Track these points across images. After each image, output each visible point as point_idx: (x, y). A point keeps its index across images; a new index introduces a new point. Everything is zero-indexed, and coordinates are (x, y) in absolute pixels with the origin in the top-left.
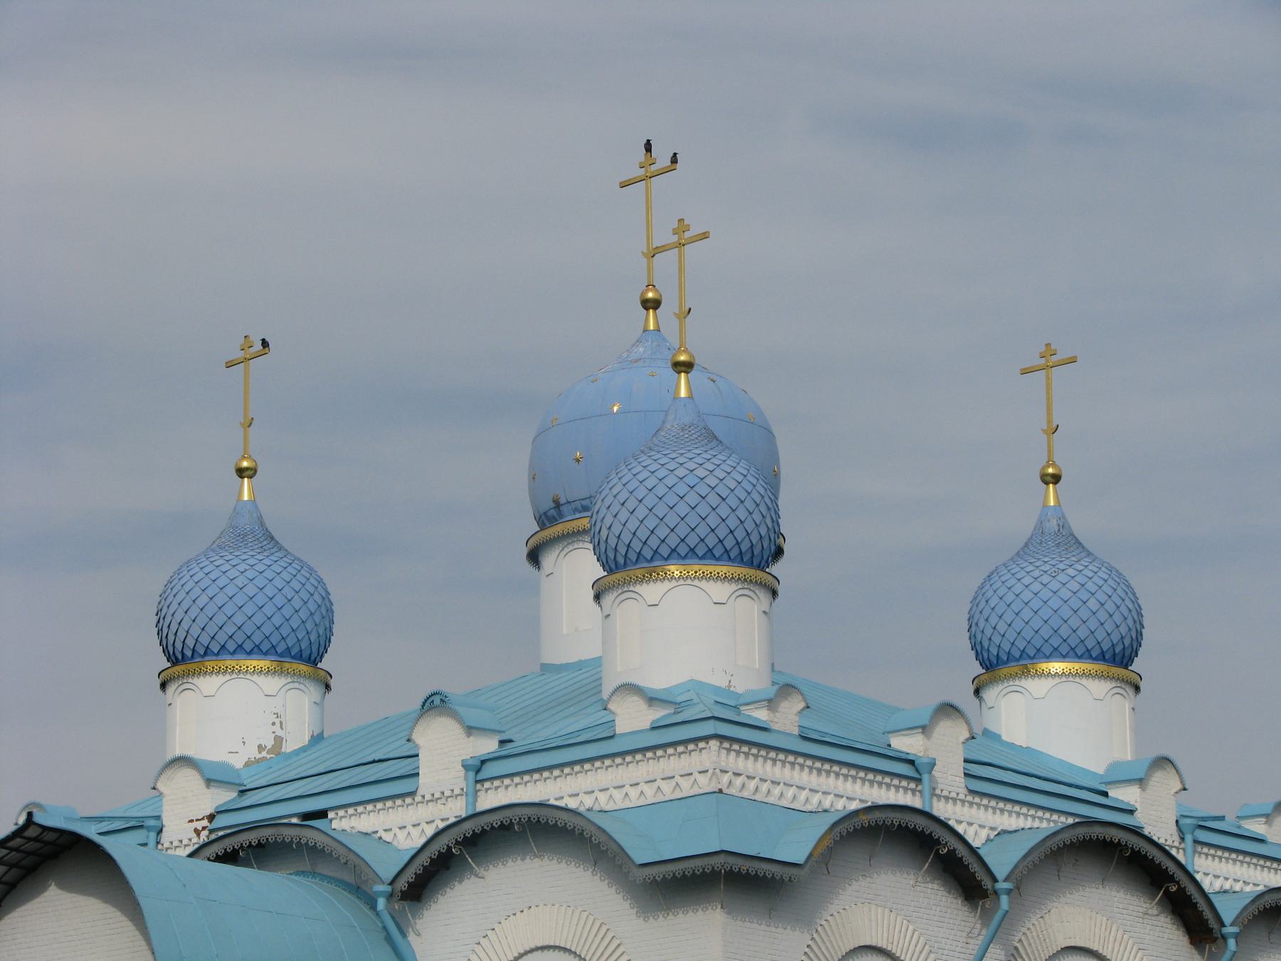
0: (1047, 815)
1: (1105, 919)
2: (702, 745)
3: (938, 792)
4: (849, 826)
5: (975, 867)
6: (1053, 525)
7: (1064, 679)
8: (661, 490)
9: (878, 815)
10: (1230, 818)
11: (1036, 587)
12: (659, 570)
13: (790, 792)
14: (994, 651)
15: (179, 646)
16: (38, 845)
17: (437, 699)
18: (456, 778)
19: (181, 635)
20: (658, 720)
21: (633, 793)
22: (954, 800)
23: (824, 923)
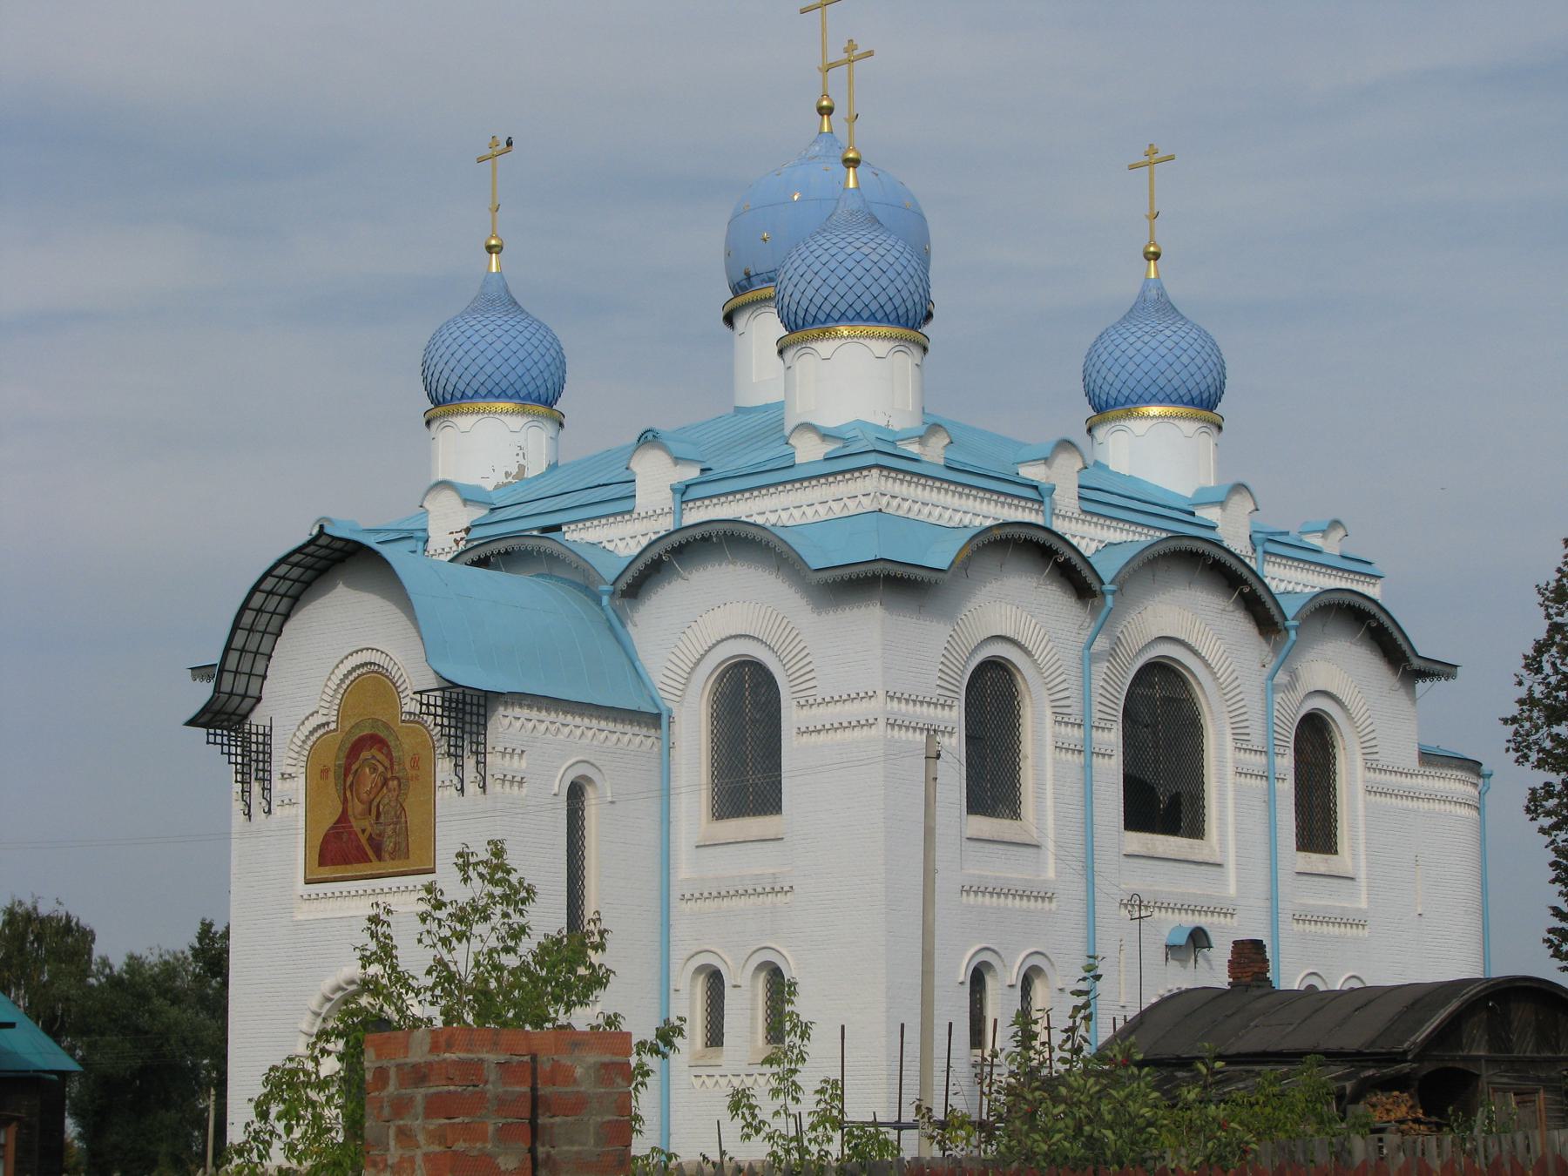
0: (1145, 531)
2: (865, 473)
3: (1057, 511)
4: (984, 539)
5: (1086, 572)
7: (1160, 420)
8: (833, 265)
10: (1294, 533)
11: (1139, 345)
13: (937, 512)
15: (440, 391)
16: (328, 551)
17: (650, 436)
18: (666, 499)
21: (810, 511)
23: (963, 617)
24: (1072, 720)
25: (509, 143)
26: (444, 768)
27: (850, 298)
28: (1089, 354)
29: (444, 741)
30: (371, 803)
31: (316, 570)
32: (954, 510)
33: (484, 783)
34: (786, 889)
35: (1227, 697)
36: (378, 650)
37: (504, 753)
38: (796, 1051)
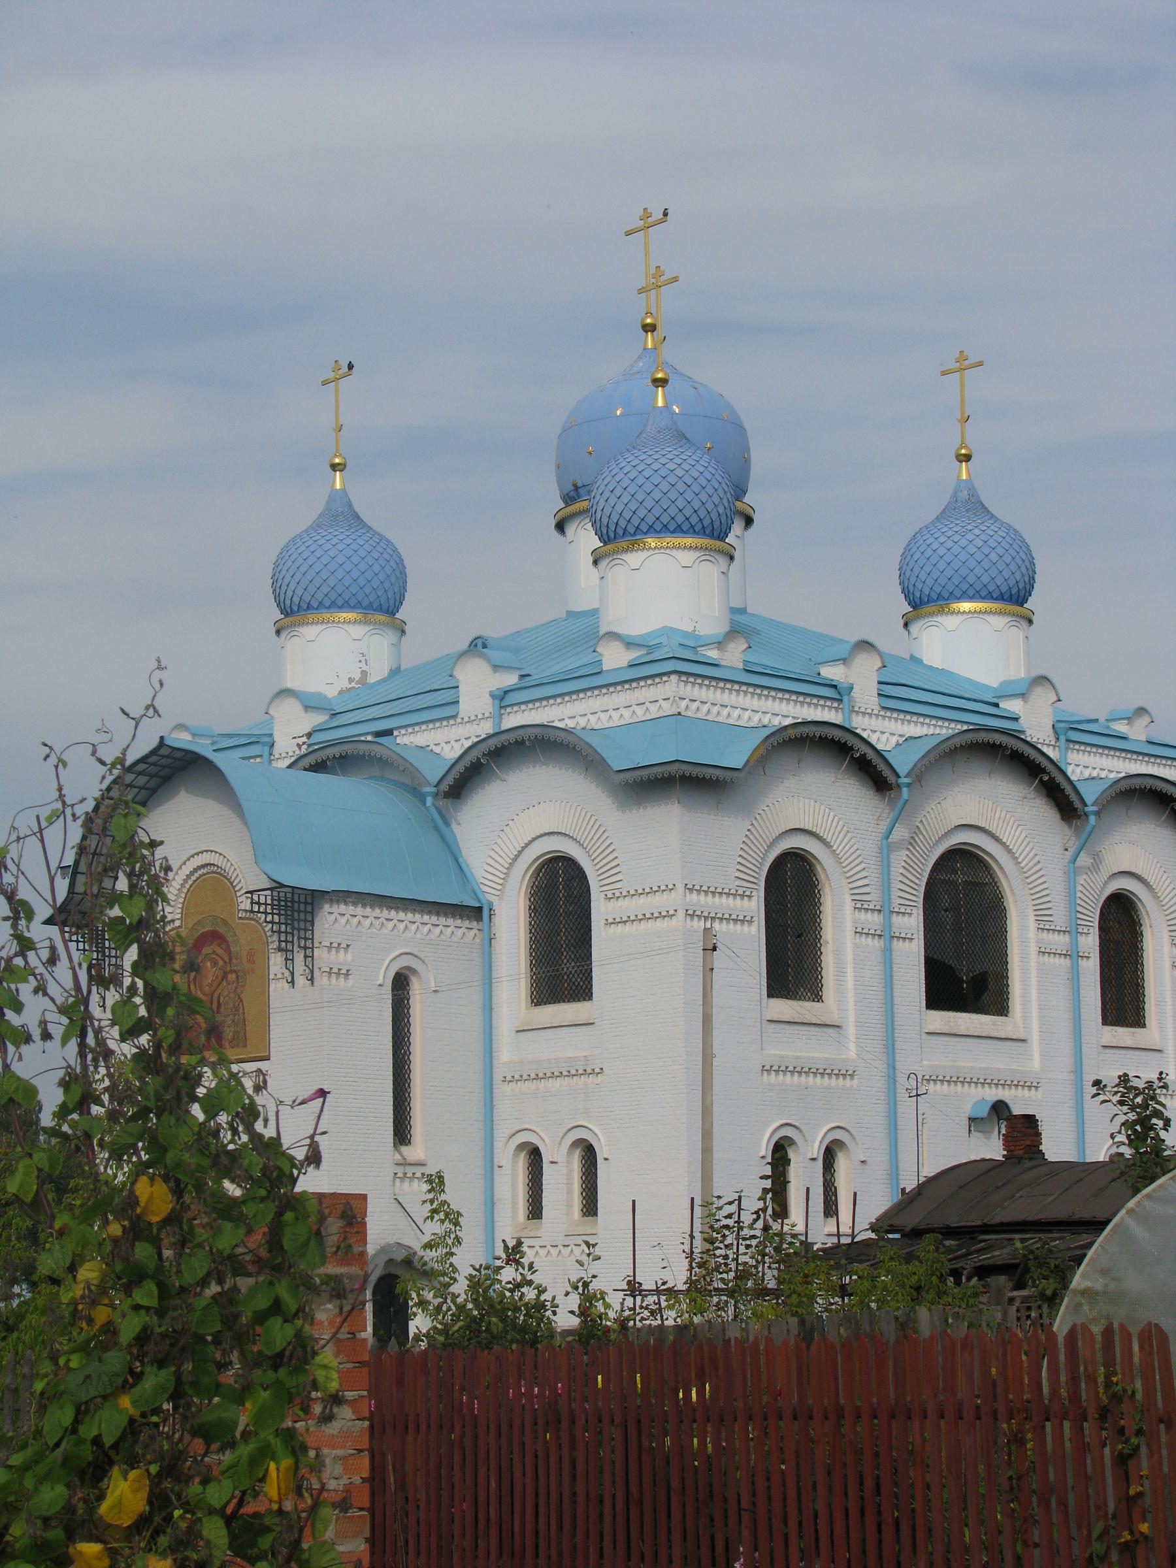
0: (946, 724)
1: (991, 803)
2: (665, 678)
3: (856, 709)
4: (779, 738)
5: (881, 767)
6: (964, 495)
7: (970, 616)
8: (640, 481)
9: (804, 730)
10: (1102, 720)
11: (949, 544)
12: (639, 542)
13: (736, 713)
14: (917, 594)
15: (288, 603)
16: (170, 761)
17: (480, 642)
18: (486, 705)
19: (289, 594)
20: (634, 659)
21: (615, 715)
22: (870, 715)
23: (761, 812)
24: (872, 907)
25: (351, 366)
26: (276, 962)
27: (657, 511)
28: (904, 553)
29: (275, 937)
30: (212, 995)
31: (160, 777)
32: (753, 711)
33: (312, 976)
34: (597, 1070)
35: (1029, 880)
36: (216, 852)
37: (330, 948)
38: (453, 1236)
